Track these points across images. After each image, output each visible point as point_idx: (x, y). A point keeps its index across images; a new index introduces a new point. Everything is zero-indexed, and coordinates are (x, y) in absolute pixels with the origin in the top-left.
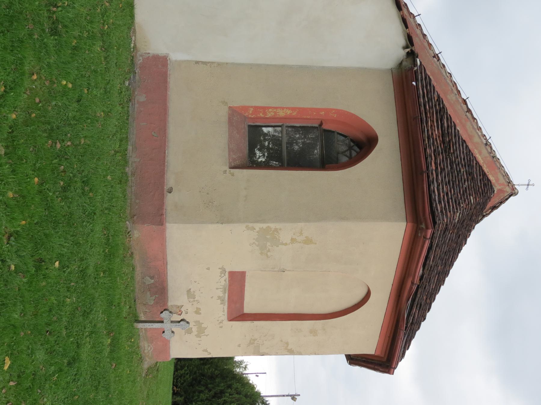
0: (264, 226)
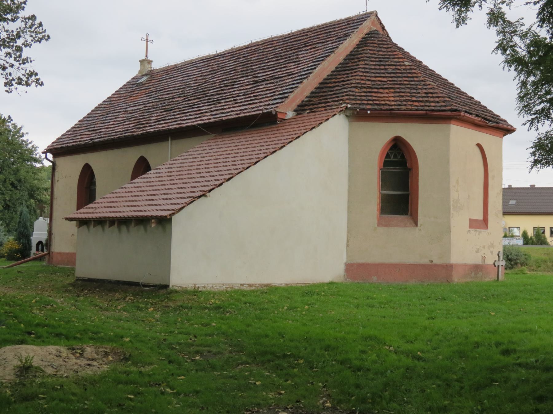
0: (452, 207)
